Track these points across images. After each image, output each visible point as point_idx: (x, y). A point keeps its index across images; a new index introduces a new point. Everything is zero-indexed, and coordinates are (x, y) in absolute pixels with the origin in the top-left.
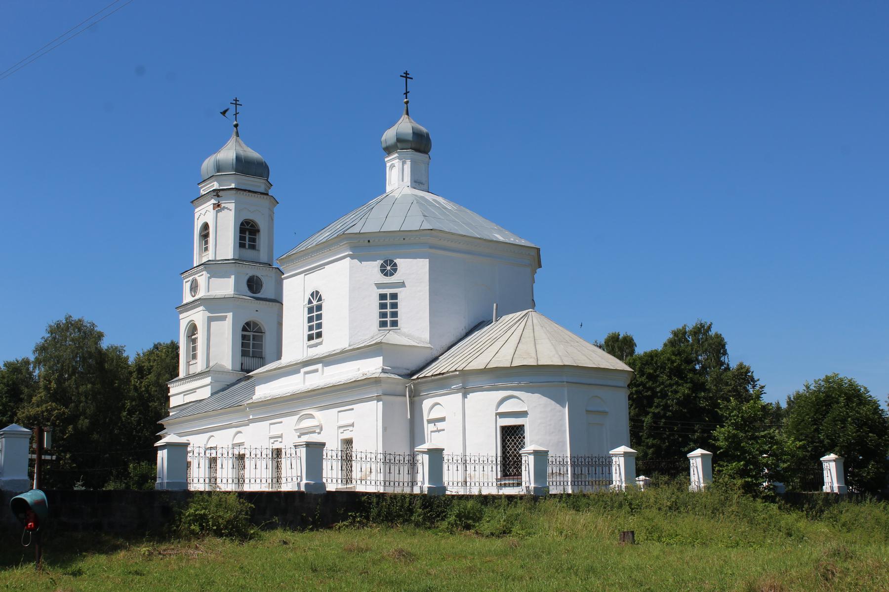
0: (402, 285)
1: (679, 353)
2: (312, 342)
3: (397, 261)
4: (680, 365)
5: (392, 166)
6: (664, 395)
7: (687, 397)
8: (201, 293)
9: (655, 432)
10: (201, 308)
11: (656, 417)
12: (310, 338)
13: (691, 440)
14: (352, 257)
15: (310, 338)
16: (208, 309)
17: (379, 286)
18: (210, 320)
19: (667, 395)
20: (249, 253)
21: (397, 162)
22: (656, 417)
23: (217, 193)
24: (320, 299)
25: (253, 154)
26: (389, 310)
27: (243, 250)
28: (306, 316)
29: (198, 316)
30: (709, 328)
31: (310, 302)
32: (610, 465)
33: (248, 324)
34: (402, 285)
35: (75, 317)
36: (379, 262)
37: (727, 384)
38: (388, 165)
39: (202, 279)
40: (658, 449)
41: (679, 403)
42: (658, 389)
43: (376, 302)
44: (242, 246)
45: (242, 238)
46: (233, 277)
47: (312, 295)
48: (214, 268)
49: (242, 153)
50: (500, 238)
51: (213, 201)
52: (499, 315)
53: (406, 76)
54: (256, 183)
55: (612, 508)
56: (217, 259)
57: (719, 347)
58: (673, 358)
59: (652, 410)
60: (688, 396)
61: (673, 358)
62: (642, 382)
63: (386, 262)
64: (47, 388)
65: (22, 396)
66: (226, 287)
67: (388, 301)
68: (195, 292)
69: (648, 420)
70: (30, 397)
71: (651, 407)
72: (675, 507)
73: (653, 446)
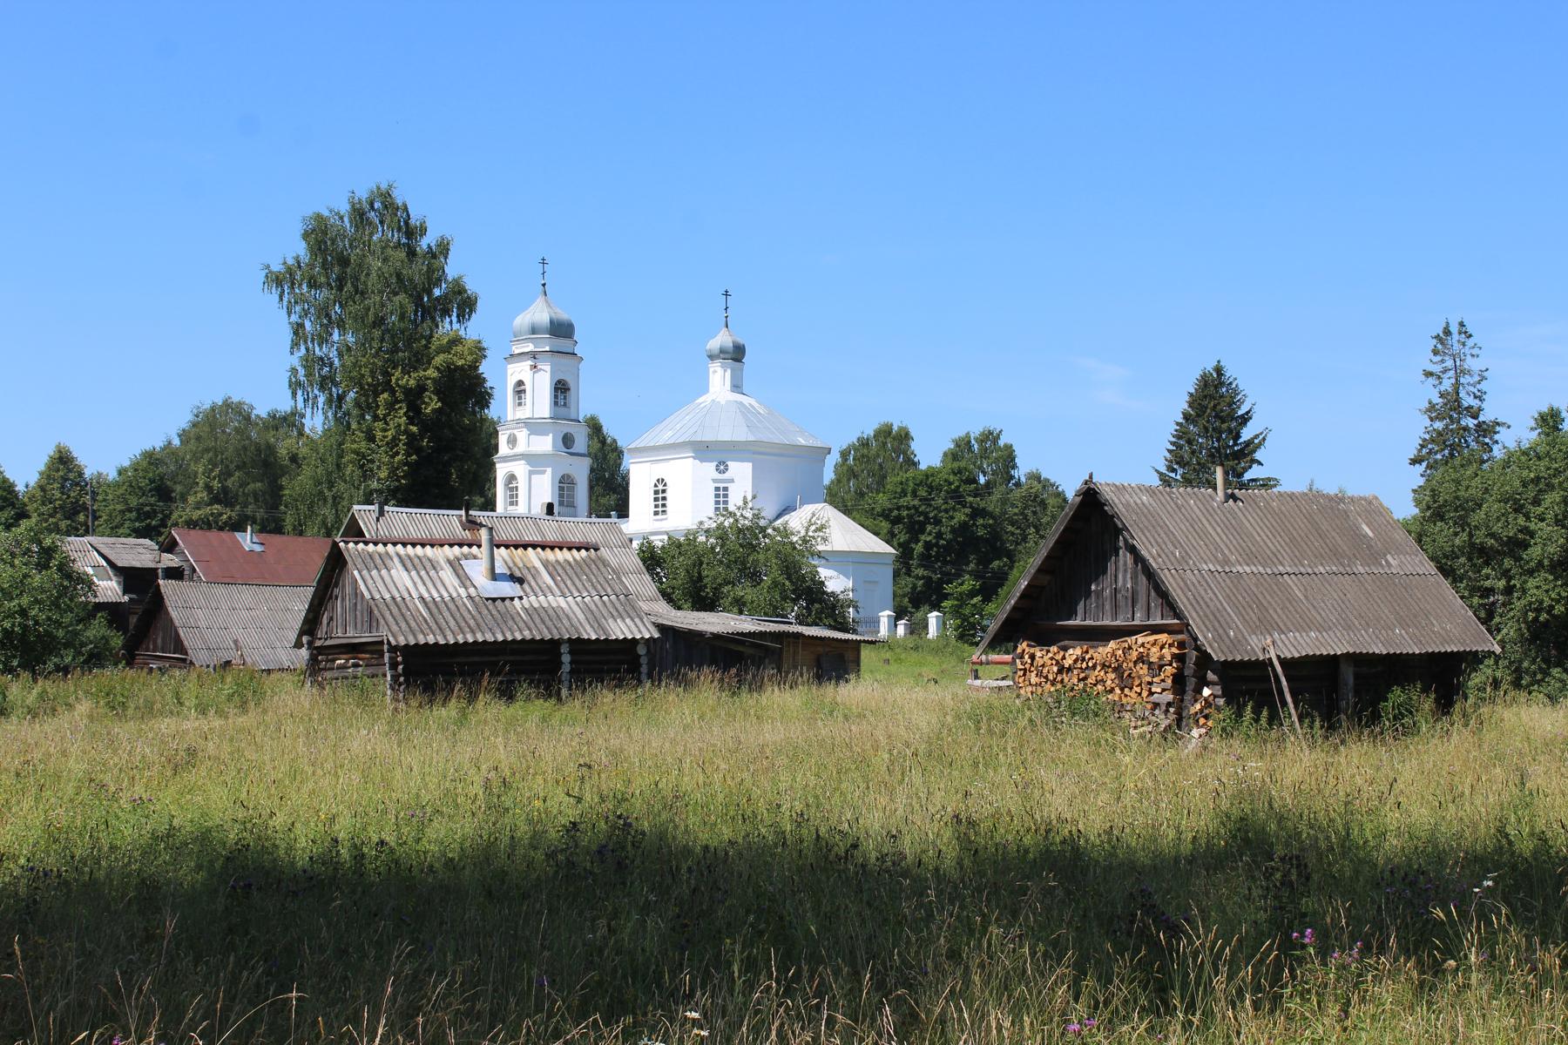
0: (732, 481)
1: (960, 472)
2: (657, 517)
3: (729, 463)
4: (958, 487)
5: (715, 372)
6: (937, 522)
7: (964, 525)
8: (521, 448)
9: (926, 560)
10: (523, 462)
11: (928, 545)
12: (656, 513)
13: (964, 571)
14: (694, 458)
15: (656, 513)
16: (529, 464)
17: (715, 481)
18: (531, 473)
19: (941, 521)
20: (562, 411)
21: (720, 371)
22: (928, 545)
23: (533, 355)
24: (665, 485)
25: (563, 315)
26: (721, 499)
27: (557, 408)
28: (653, 496)
29: (520, 469)
30: (998, 437)
31: (656, 486)
32: (879, 622)
33: (563, 477)
34: (732, 481)
35: (235, 399)
36: (715, 463)
37: (1013, 505)
38: (711, 370)
39: (522, 435)
40: (928, 580)
41: (953, 530)
42: (932, 515)
43: (713, 493)
44: (556, 403)
45: (556, 397)
46: (551, 435)
47: (658, 481)
48: (533, 426)
49: (554, 316)
50: (803, 442)
51: (530, 362)
52: (802, 504)
53: (726, 294)
54: (563, 344)
55: (1291, 859)
56: (535, 416)
57: (1008, 459)
58: (952, 478)
59: (923, 537)
60: (965, 522)
61: (952, 478)
62: (914, 505)
63: (720, 463)
64: (208, 488)
65: (173, 495)
66: (545, 444)
67: (722, 493)
68: (514, 446)
69: (918, 548)
70: (184, 499)
71: (923, 534)
72: (916, 648)
73: (923, 577)
